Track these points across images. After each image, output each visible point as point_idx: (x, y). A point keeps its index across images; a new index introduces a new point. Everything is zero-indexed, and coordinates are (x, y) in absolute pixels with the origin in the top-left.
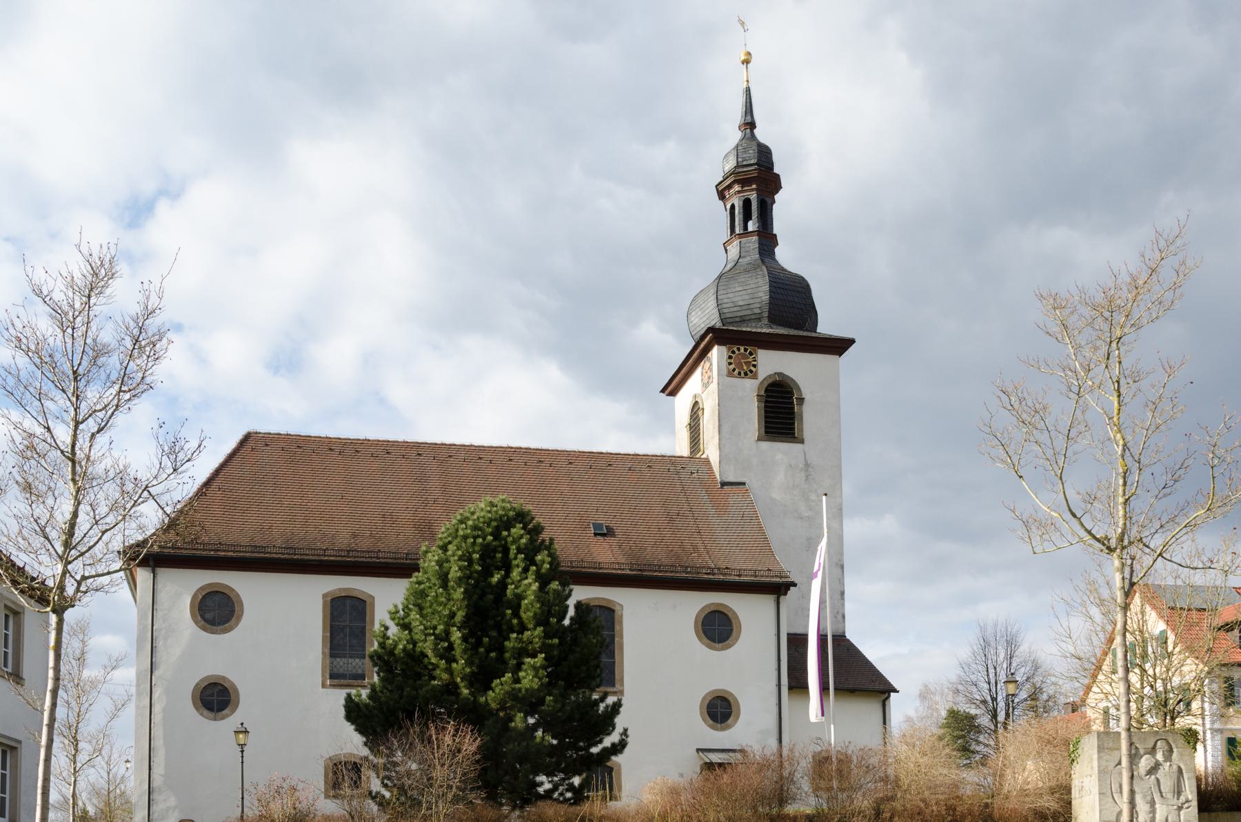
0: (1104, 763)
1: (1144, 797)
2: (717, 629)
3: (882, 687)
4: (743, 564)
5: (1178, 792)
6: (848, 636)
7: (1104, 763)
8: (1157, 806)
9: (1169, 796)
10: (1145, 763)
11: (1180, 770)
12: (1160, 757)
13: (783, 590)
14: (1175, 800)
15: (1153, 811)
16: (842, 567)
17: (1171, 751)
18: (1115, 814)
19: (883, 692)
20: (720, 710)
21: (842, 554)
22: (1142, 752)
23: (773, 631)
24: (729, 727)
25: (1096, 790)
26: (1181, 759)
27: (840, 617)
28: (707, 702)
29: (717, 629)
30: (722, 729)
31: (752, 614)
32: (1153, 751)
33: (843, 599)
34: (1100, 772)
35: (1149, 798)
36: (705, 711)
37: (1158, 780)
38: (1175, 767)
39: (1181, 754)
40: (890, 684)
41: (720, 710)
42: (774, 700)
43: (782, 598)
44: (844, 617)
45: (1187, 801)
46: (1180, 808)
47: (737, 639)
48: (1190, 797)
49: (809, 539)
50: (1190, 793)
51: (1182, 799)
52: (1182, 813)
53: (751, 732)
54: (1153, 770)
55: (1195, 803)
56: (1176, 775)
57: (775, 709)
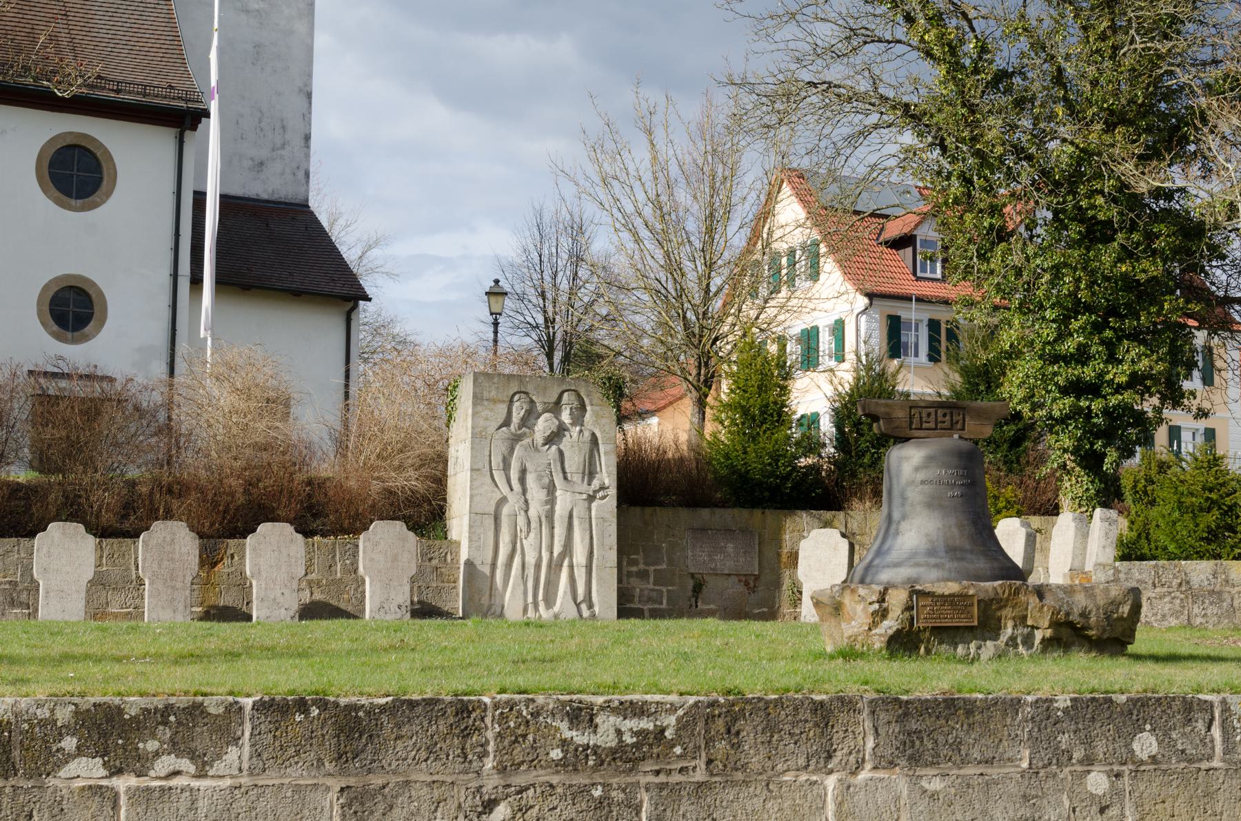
0: (482, 423)
1: (540, 478)
2: (76, 176)
3: (345, 291)
4: (133, 74)
5: (590, 472)
6: (313, 204)
7: (482, 423)
8: (558, 493)
9: (576, 478)
10: (544, 425)
11: (594, 440)
12: (566, 417)
13: (188, 121)
14: (584, 487)
15: (551, 501)
16: (309, 96)
17: (583, 408)
18: (493, 503)
19: (346, 299)
20: (72, 308)
21: (310, 75)
22: (540, 408)
23: (171, 186)
24: (86, 338)
25: (468, 465)
26: (596, 422)
27: (301, 174)
28: (51, 294)
29: (76, 176)
30: (75, 341)
31: (135, 153)
32: (555, 408)
33: (308, 147)
34: (474, 436)
35: (546, 480)
36: (46, 308)
37: (561, 453)
38: (587, 434)
39: (597, 415)
40: (360, 288)
41: (72, 308)
42: (166, 299)
43: (188, 133)
44: (307, 175)
45: (602, 488)
46: (591, 498)
47: (109, 194)
48: (607, 482)
49: (257, 46)
50: (607, 475)
51: (596, 484)
52: (594, 505)
53: (120, 349)
54: (554, 437)
55: (613, 492)
56: (587, 447)
57: (166, 314)
